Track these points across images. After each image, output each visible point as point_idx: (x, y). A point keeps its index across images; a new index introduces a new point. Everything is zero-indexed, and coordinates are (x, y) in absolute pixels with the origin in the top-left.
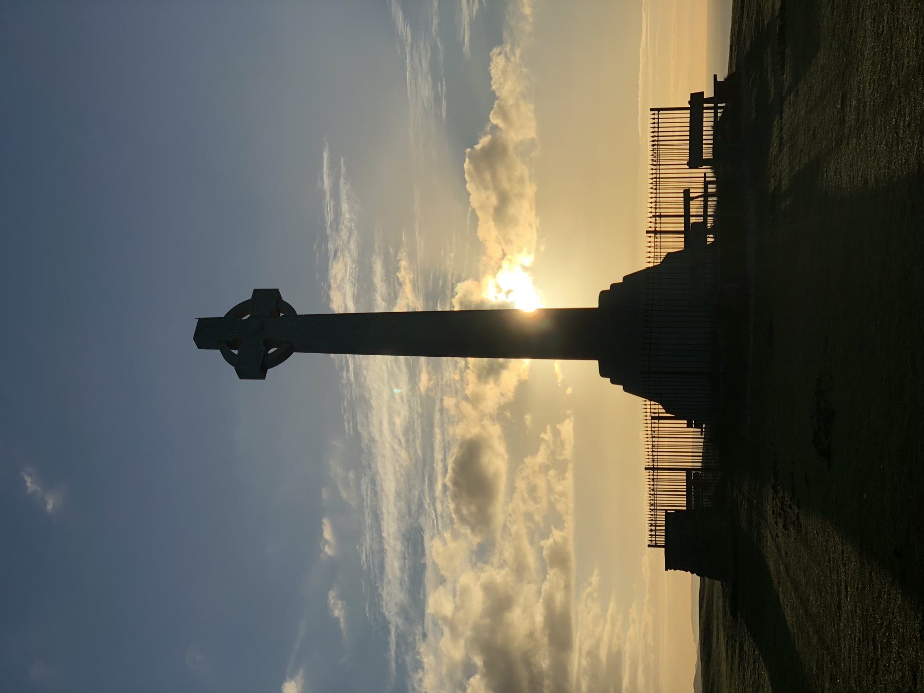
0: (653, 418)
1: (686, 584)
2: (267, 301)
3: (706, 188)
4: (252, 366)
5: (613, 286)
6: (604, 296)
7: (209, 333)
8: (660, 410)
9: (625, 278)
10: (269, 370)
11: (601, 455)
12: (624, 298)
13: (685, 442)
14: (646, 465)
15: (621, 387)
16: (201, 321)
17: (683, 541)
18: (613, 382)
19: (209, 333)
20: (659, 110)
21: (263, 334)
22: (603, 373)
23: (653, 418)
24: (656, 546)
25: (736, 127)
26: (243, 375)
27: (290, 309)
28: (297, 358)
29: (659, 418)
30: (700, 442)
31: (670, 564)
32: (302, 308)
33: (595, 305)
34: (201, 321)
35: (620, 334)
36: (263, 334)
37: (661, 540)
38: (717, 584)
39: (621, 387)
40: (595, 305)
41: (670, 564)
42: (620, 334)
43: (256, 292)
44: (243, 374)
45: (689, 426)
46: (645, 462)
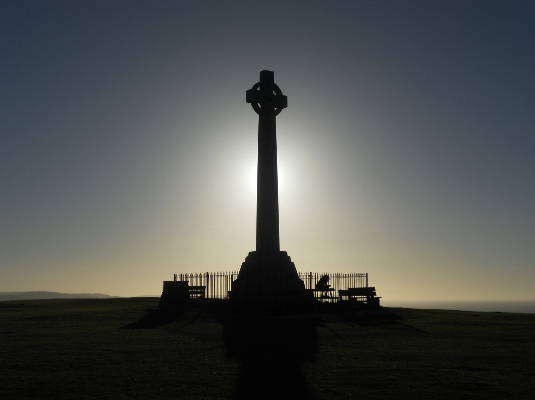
0: (232, 276)
1: (157, 292)
2: (281, 102)
3: (335, 298)
4: (252, 97)
5: (289, 257)
7: (267, 77)
8: (235, 278)
9: (293, 263)
12: (285, 263)
13: (220, 290)
14: (209, 273)
15: (254, 249)
17: (176, 290)
18: (247, 258)
19: (267, 77)
20: (367, 277)
21: (267, 101)
23: (232, 276)
24: (175, 277)
27: (278, 112)
28: (257, 116)
29: (232, 278)
30: (223, 297)
31: (166, 284)
33: (281, 250)
35: (268, 263)
36: (267, 101)
37: (177, 280)
39: (254, 249)
40: (281, 250)
41: (166, 284)
42: (268, 263)
44: (249, 93)
45: (228, 292)
46: (211, 271)
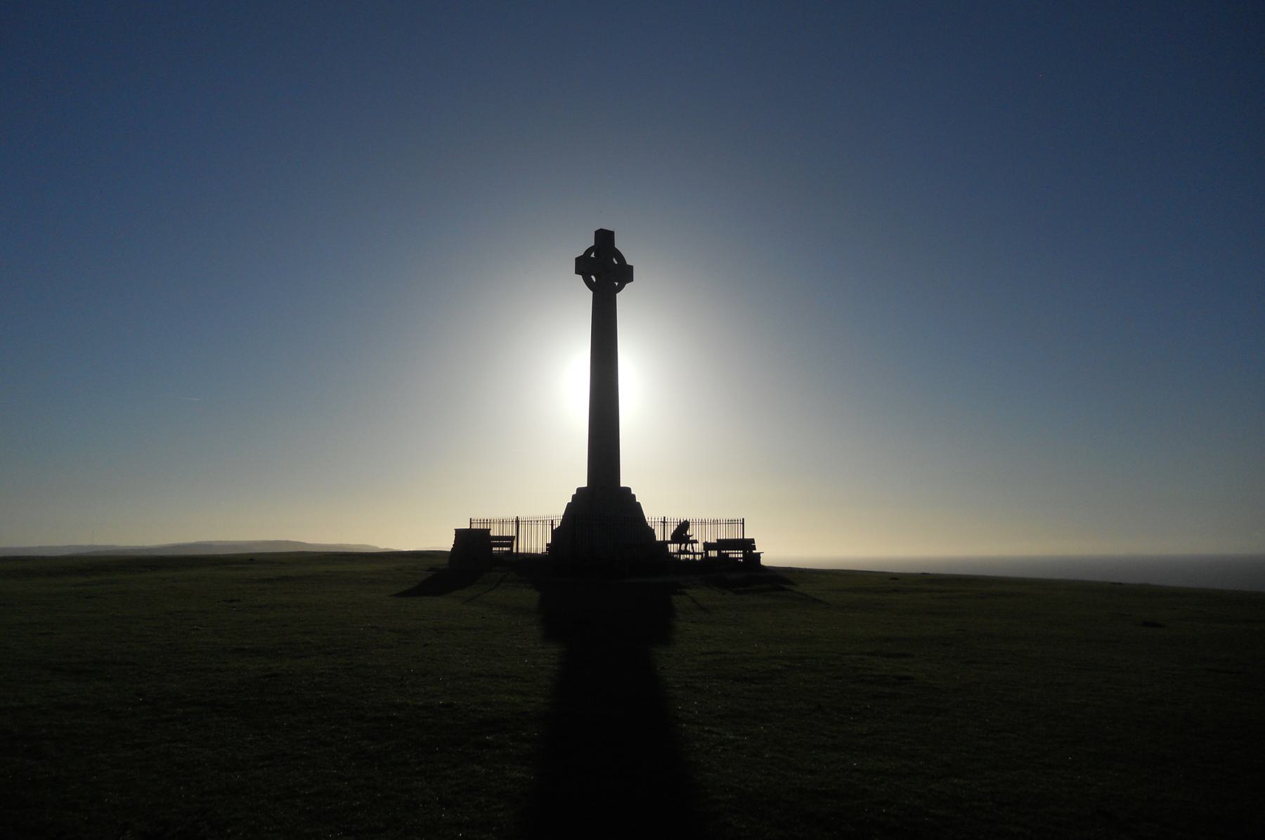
1: (446, 543)
2: (625, 274)
4: (584, 266)
6: (627, 490)
7: (604, 239)
8: (557, 524)
10: (584, 483)
11: (532, 494)
13: (535, 542)
16: (612, 233)
17: (473, 541)
19: (604, 239)
21: (604, 271)
22: (579, 490)
25: (735, 566)
26: (578, 260)
27: (620, 288)
28: (589, 294)
30: (539, 552)
31: (459, 533)
32: (620, 297)
34: (612, 233)
35: (603, 504)
36: (604, 271)
37: (475, 526)
38: (446, 561)
41: (459, 533)
42: (603, 504)
43: (631, 267)
